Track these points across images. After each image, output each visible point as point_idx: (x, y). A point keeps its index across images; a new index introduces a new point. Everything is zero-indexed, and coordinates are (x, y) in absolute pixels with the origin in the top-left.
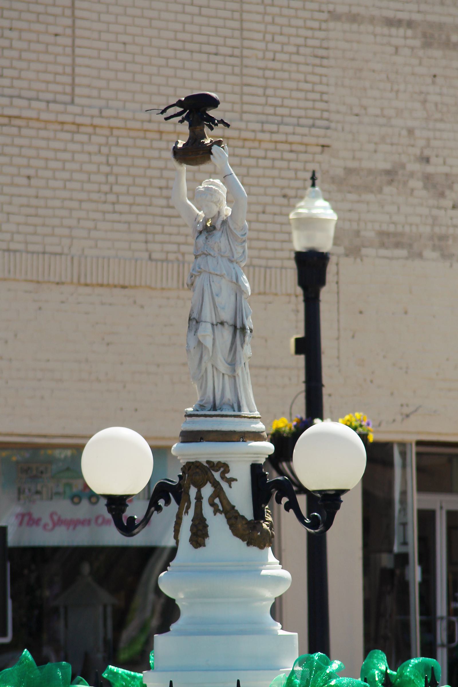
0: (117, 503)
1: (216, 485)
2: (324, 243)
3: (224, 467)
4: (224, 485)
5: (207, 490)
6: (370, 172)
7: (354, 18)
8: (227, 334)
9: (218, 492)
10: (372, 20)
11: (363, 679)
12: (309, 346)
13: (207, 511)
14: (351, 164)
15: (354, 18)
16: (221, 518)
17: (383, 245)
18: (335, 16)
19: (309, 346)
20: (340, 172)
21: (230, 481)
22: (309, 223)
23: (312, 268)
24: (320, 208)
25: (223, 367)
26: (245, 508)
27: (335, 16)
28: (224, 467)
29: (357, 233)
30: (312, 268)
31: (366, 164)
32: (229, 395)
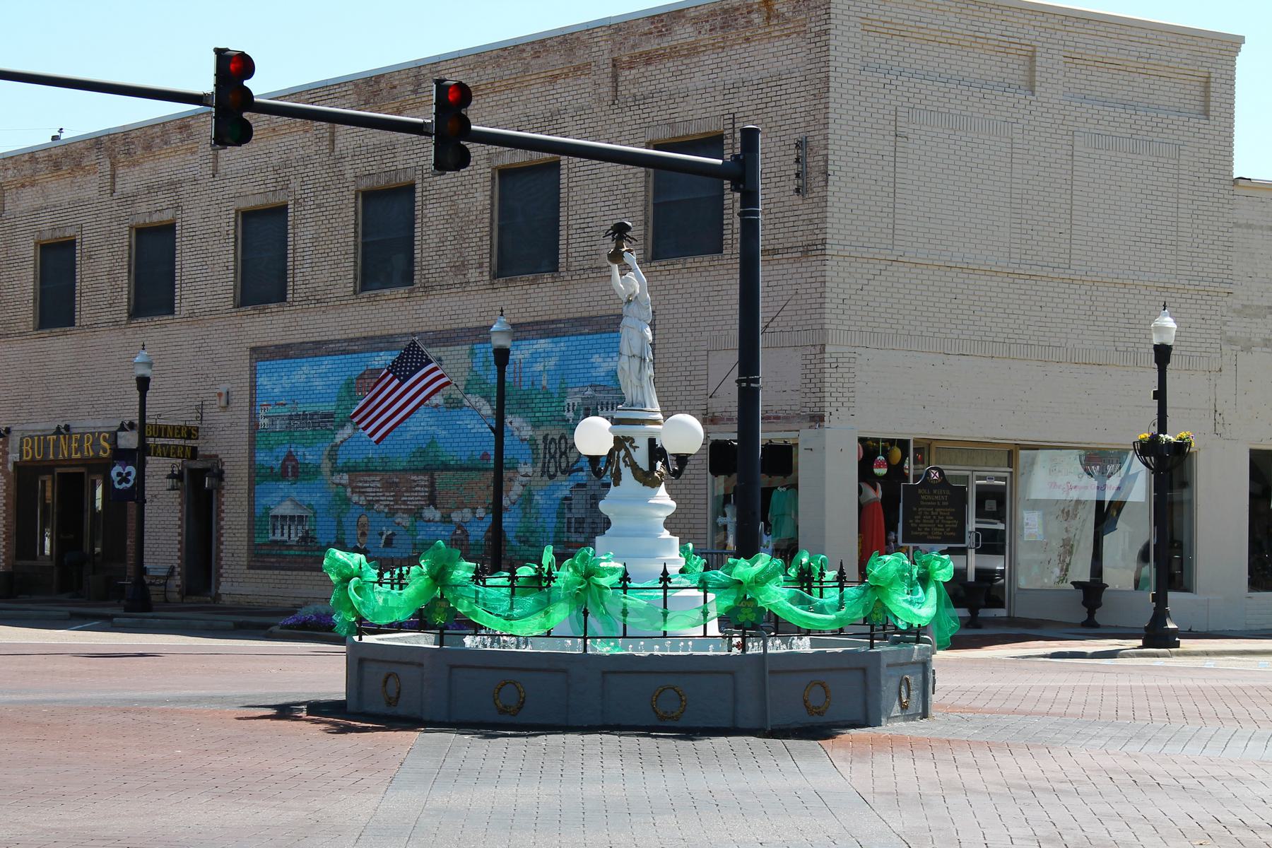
0: (594, 460)
1: (627, 450)
2: (1170, 341)
3: (632, 440)
4: (631, 450)
5: (622, 453)
6: (1258, 307)
7: (1249, 226)
8: (636, 362)
9: (628, 454)
10: (1261, 227)
11: (435, 572)
12: (1160, 395)
13: (622, 465)
14: (1245, 303)
15: (1249, 226)
16: (629, 469)
17: (1266, 346)
18: (1236, 225)
19: (1160, 395)
20: (1239, 307)
21: (635, 448)
22: (1162, 330)
23: (1163, 354)
24: (1168, 322)
25: (635, 381)
26: (643, 463)
27: (1236, 225)
28: (632, 440)
29: (1250, 339)
30: (1163, 354)
31: (1255, 303)
32: (640, 398)
